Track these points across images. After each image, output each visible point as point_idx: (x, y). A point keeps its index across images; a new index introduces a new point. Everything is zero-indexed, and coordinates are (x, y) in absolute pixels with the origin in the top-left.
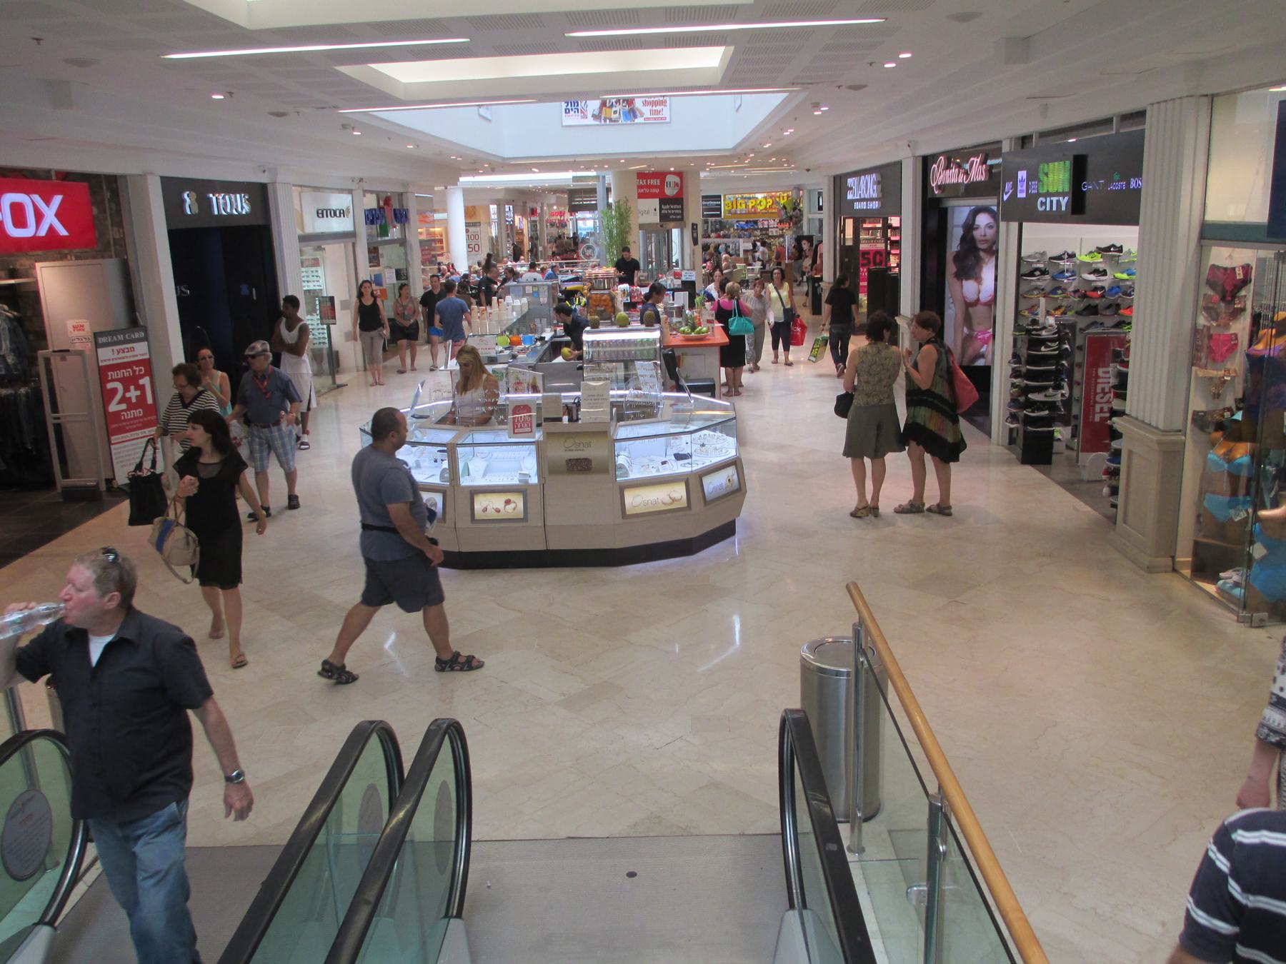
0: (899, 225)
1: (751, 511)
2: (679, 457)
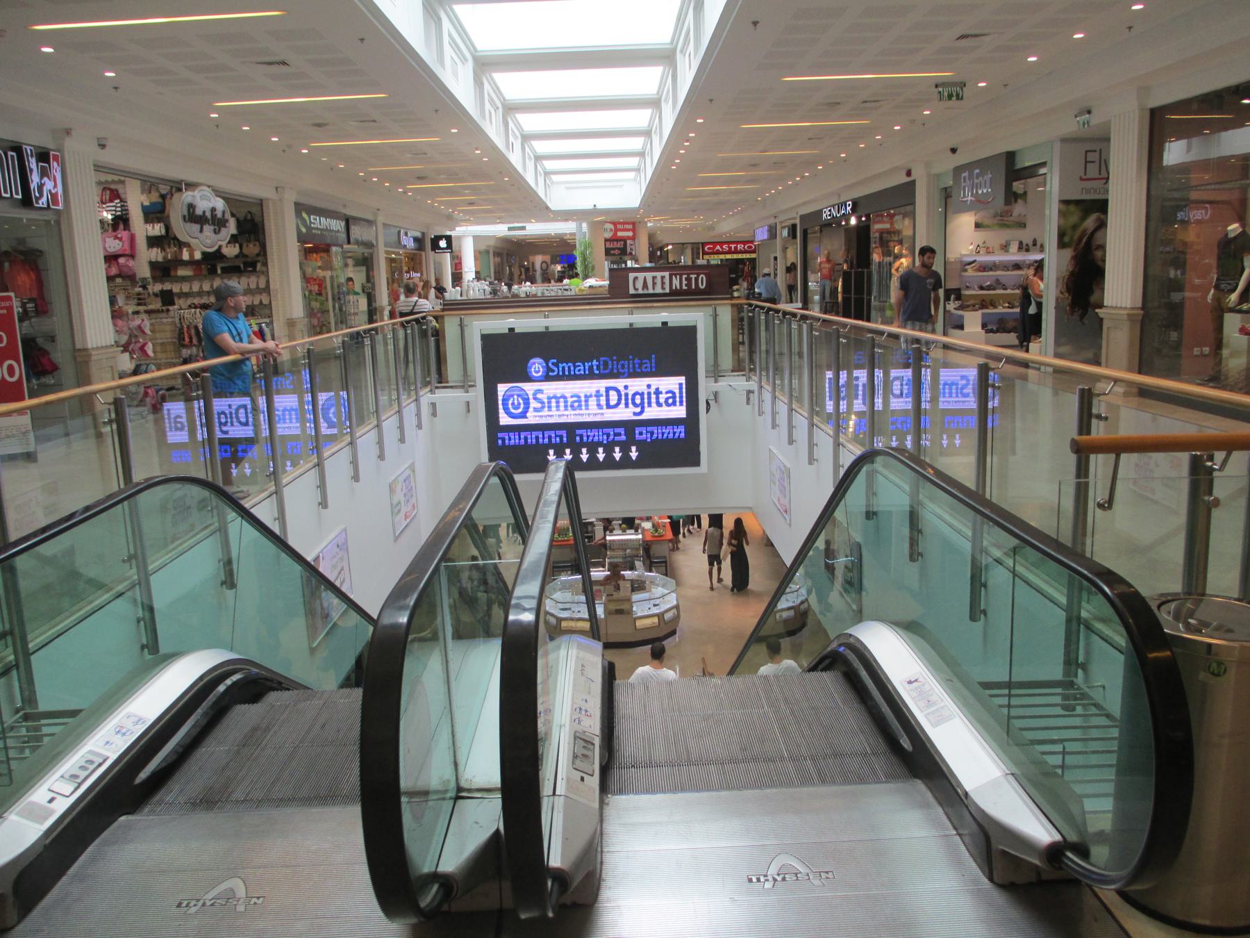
0: (1184, 457)
1: (683, 624)
2: (655, 605)
